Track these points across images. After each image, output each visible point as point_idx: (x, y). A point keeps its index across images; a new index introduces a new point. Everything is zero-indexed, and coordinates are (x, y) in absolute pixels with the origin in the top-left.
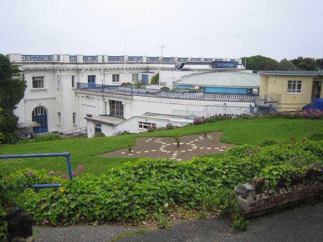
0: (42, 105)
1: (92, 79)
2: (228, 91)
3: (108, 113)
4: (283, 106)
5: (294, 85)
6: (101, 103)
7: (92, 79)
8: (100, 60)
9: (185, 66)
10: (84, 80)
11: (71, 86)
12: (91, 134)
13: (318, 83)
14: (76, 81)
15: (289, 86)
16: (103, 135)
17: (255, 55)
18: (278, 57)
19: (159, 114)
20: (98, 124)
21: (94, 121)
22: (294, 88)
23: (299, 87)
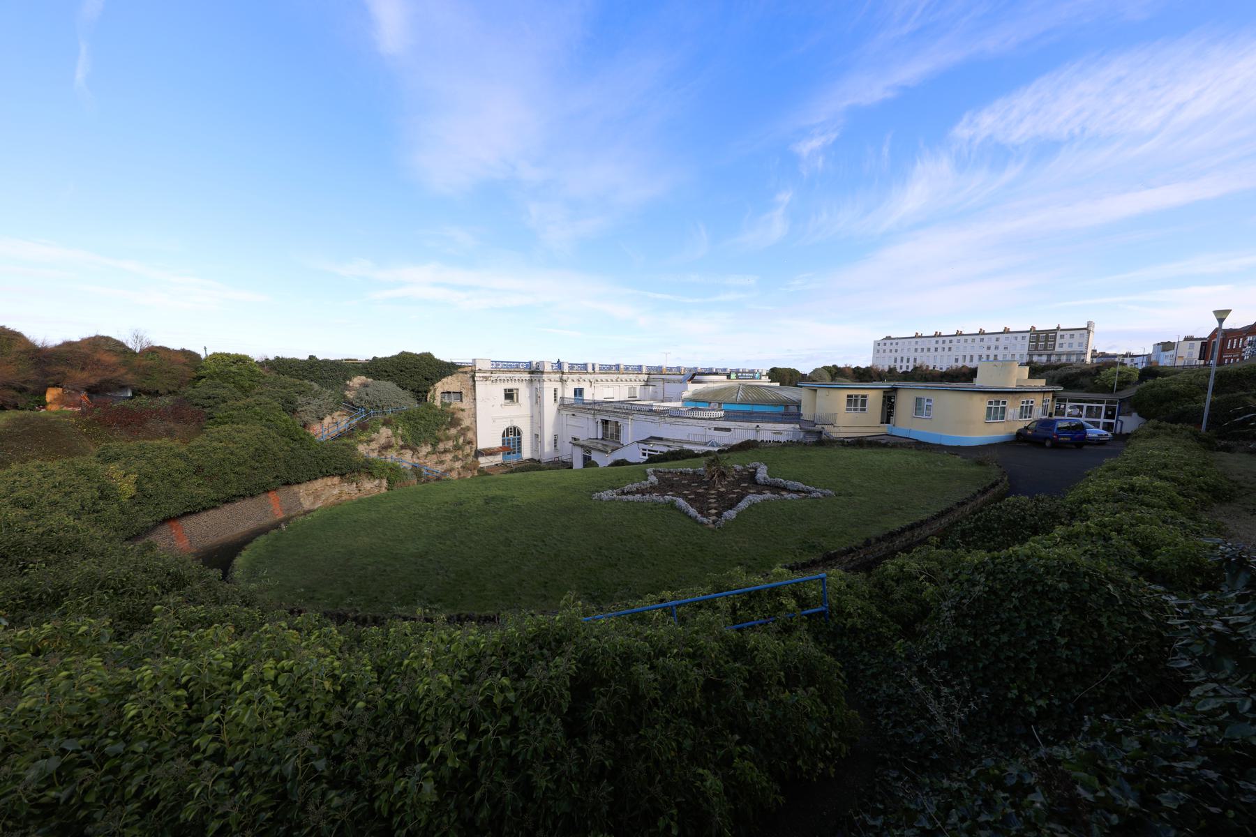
0: (918, 363)
1: (579, 392)
2: (757, 409)
3: (600, 436)
4: (842, 429)
5: (856, 401)
6: (592, 424)
7: (579, 392)
8: (590, 370)
9: (696, 377)
10: (569, 394)
11: (1189, 334)
12: (578, 464)
13: (890, 398)
14: (559, 395)
15: (849, 402)
16: (595, 464)
17: (232, 350)
18: (805, 369)
19: (661, 439)
20: (587, 449)
21: (582, 446)
22: (856, 405)
23: (864, 403)
